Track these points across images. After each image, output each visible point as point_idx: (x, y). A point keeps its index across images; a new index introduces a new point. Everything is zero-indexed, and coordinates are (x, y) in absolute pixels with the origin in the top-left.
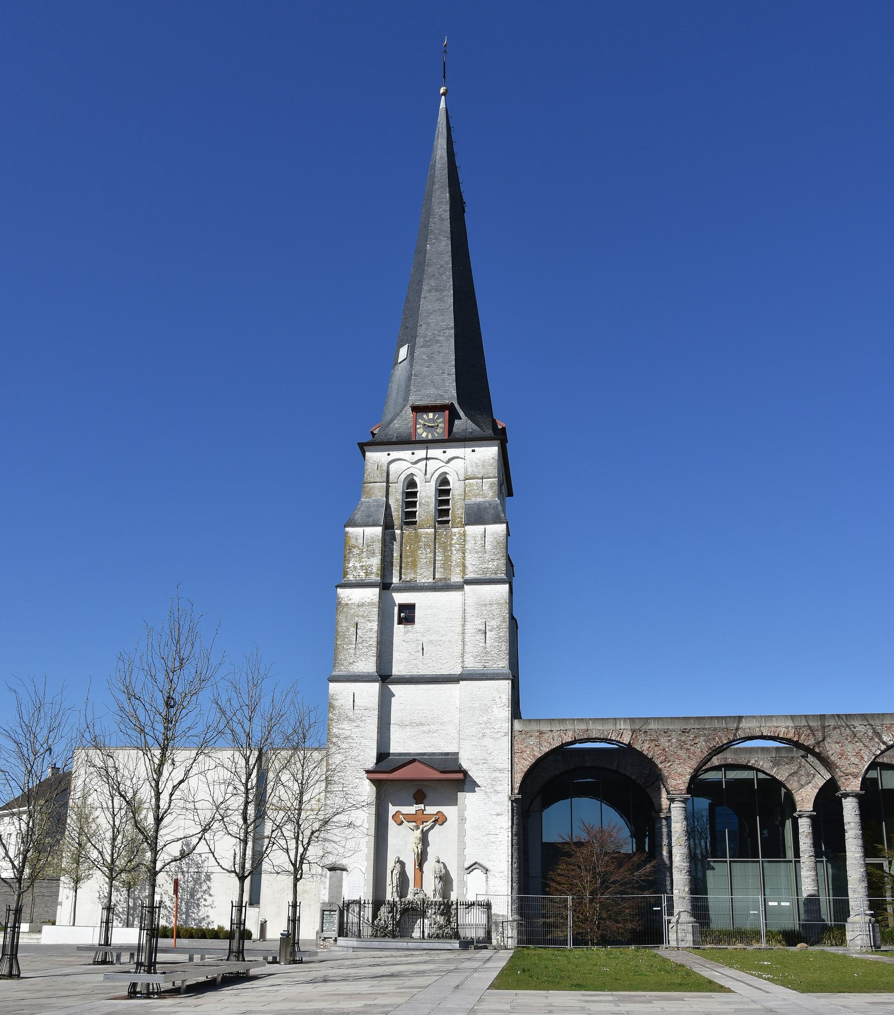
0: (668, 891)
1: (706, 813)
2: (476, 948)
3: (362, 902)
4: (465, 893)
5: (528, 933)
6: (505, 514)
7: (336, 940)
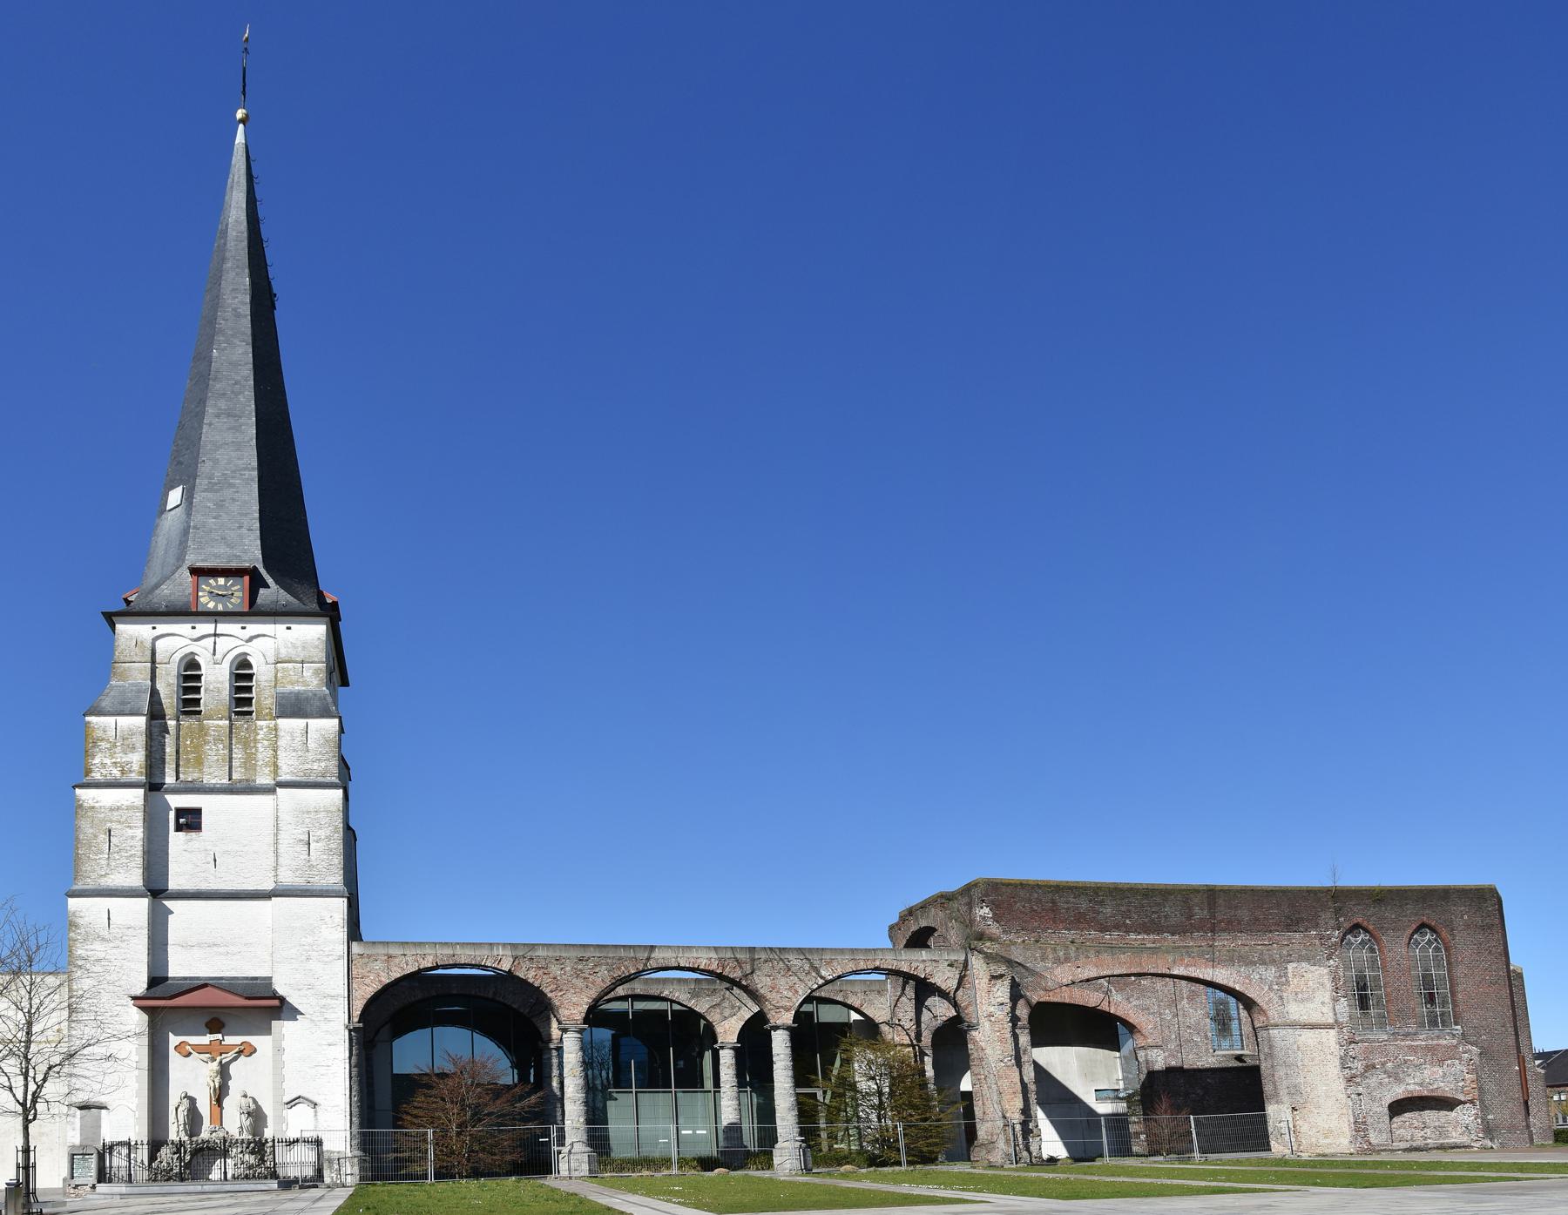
0: (559, 1122)
1: (608, 1044)
2: (301, 1187)
3: (133, 1143)
4: (284, 1129)
5: (373, 1169)
6: (337, 707)
7: (94, 1187)
